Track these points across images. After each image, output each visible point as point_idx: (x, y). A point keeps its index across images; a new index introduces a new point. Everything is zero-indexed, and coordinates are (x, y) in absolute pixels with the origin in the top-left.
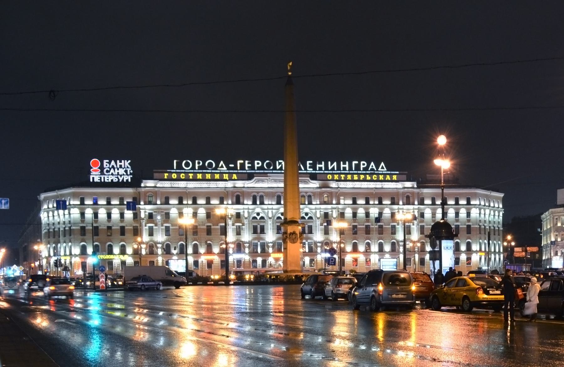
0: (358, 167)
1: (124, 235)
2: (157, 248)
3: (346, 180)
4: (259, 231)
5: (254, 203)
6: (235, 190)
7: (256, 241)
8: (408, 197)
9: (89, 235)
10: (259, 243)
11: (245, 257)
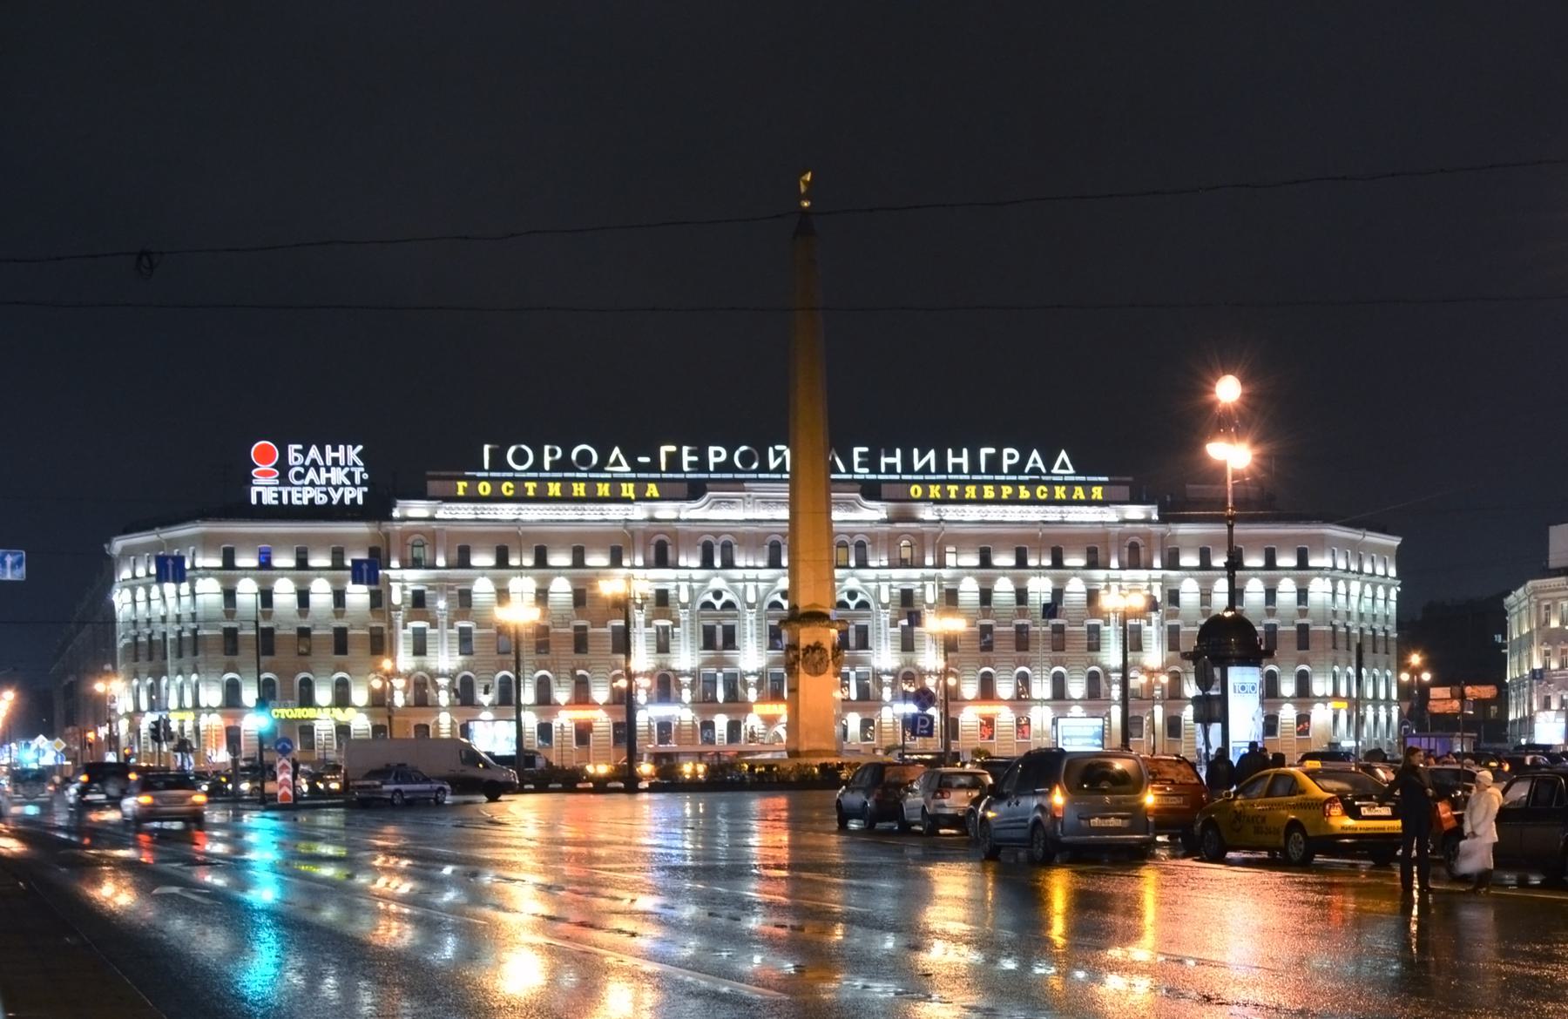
0: (994, 464)
1: (345, 652)
2: (437, 688)
3: (961, 500)
4: (720, 641)
5: (707, 563)
6: (654, 527)
7: (712, 670)
8: (1134, 548)
10: (720, 675)
11: (682, 713)
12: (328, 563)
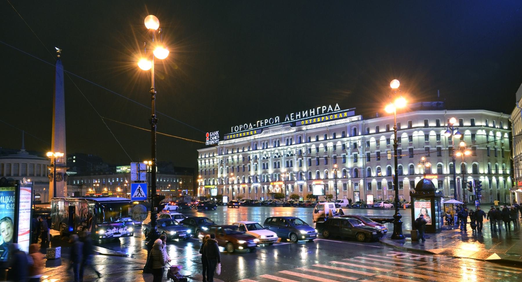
0: (320, 110)
9: (500, 158)
11: (259, 185)
12: (470, 124)
